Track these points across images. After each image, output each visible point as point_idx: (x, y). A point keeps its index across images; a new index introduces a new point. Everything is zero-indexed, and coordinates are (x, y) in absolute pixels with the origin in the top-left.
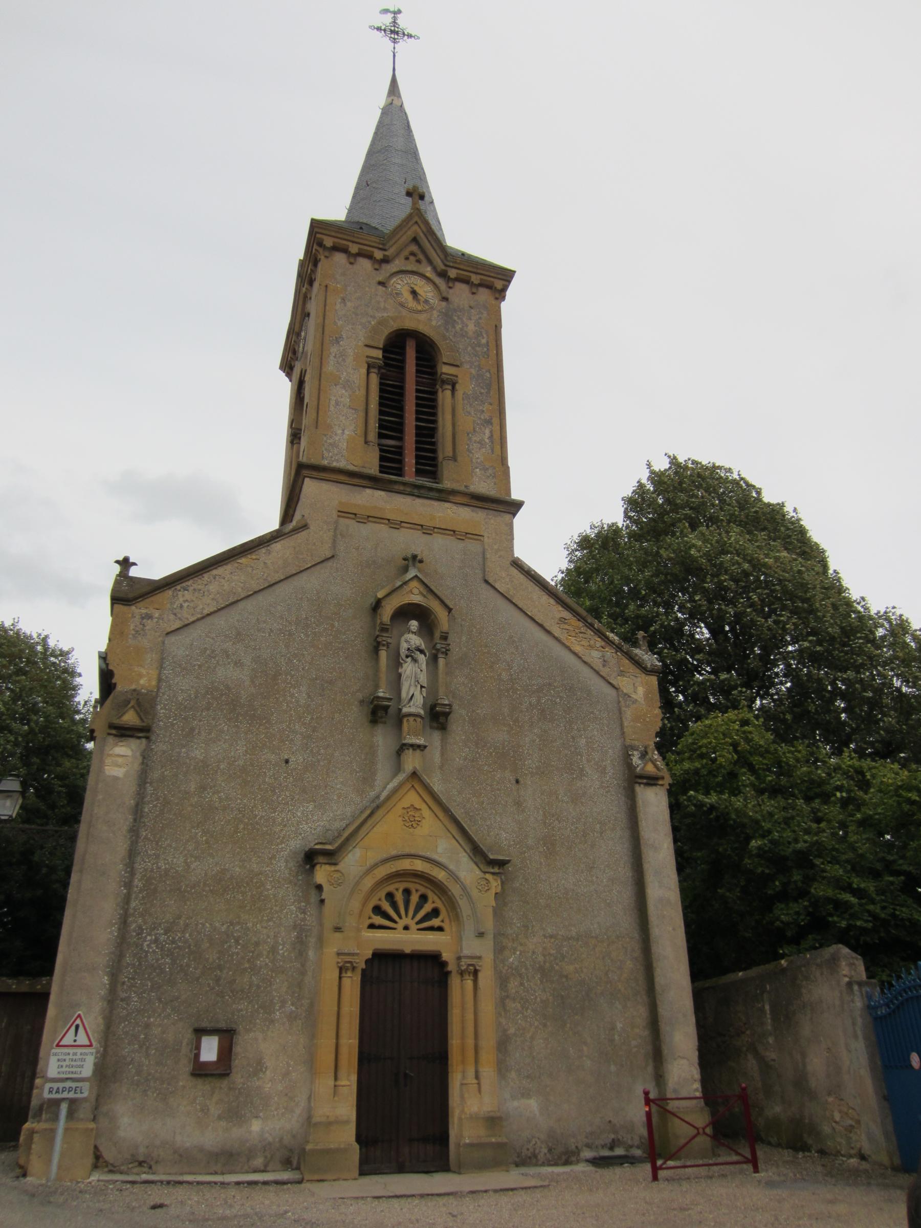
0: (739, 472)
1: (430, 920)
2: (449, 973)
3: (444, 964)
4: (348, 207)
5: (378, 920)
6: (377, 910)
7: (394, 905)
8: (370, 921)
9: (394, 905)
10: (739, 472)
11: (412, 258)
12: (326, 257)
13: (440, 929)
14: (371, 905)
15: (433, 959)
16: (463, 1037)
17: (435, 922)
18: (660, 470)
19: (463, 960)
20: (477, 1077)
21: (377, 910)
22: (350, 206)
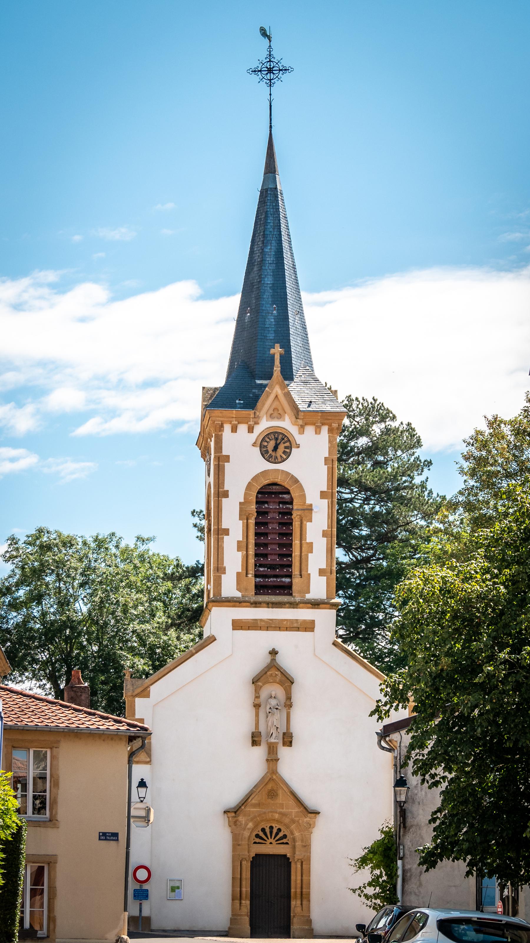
0: (363, 398)
1: (282, 839)
2: (291, 862)
3: (289, 859)
4: (236, 318)
5: (258, 840)
6: (257, 836)
7: (265, 834)
8: (254, 841)
9: (265, 834)
10: (363, 398)
11: (276, 414)
12: (481, 433)
13: (287, 843)
14: (254, 834)
15: (284, 857)
16: (296, 888)
17: (285, 841)
18: (318, 431)
19: (269, 556)
20: (302, 904)
21: (257, 836)
22: (238, 317)
